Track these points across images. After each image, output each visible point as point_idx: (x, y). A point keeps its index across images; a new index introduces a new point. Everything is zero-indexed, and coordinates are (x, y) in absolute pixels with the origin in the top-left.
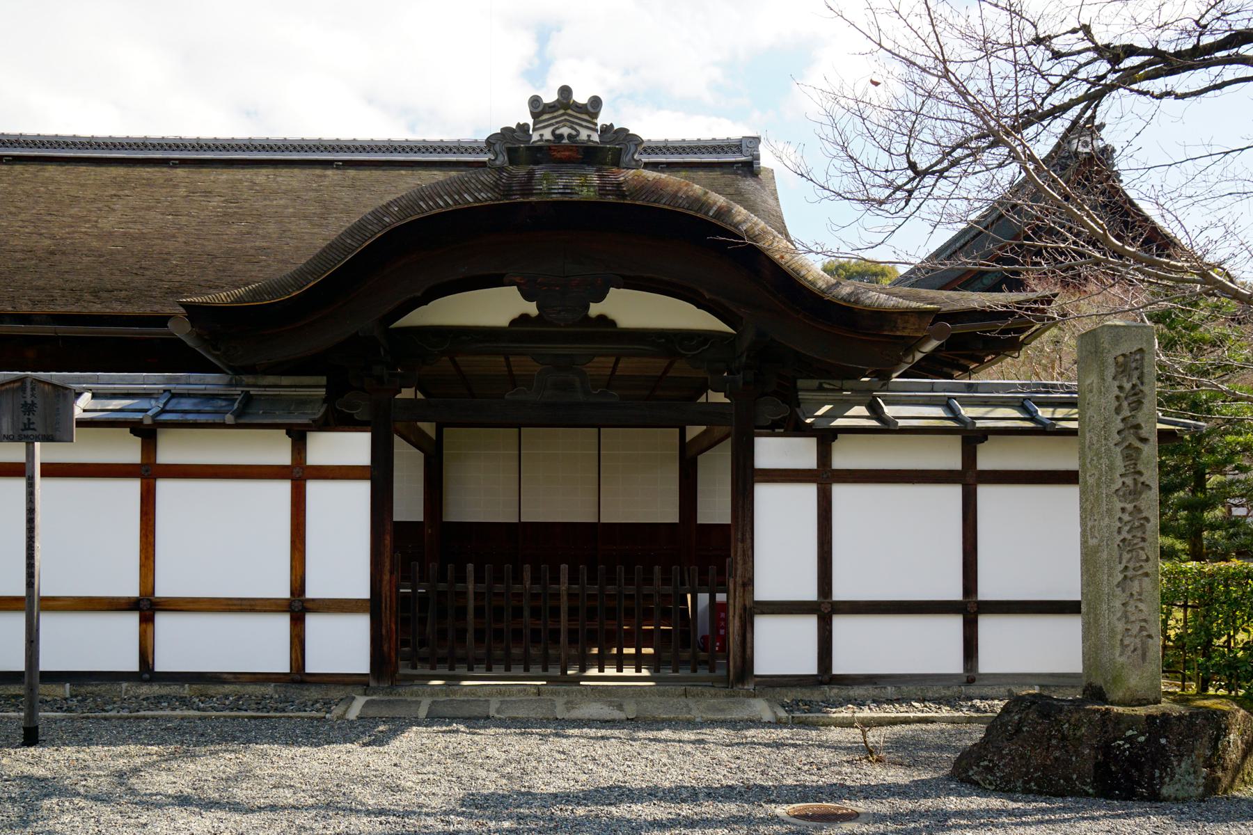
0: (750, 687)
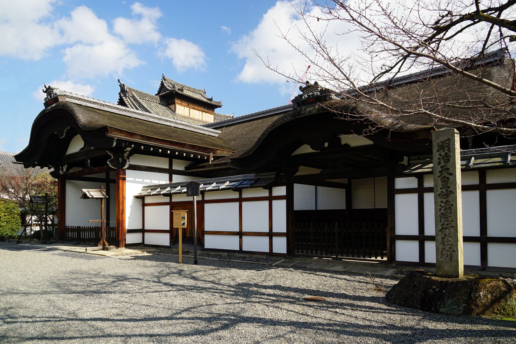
0: (394, 265)
